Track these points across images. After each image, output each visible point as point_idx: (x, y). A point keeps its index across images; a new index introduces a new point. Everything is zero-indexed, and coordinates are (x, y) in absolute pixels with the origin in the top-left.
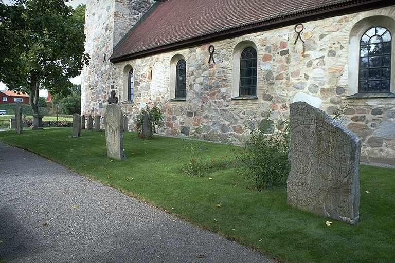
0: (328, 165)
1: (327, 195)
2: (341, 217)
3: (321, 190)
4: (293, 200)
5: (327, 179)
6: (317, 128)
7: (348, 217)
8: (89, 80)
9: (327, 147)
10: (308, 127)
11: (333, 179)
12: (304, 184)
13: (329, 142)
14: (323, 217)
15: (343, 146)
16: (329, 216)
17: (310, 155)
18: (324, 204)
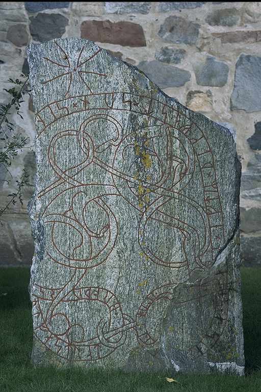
0: (169, 224)
1: (170, 309)
2: (211, 364)
3: (151, 299)
4: (55, 349)
5: (167, 264)
6: (133, 118)
7: (231, 360)
8: (169, 235)
9: (168, 174)
10: (102, 117)
11: (186, 263)
12: (93, 293)
13: (171, 157)
14: (113, 374)
15: (213, 166)
16: (177, 368)
17: (112, 199)
18: (163, 339)
